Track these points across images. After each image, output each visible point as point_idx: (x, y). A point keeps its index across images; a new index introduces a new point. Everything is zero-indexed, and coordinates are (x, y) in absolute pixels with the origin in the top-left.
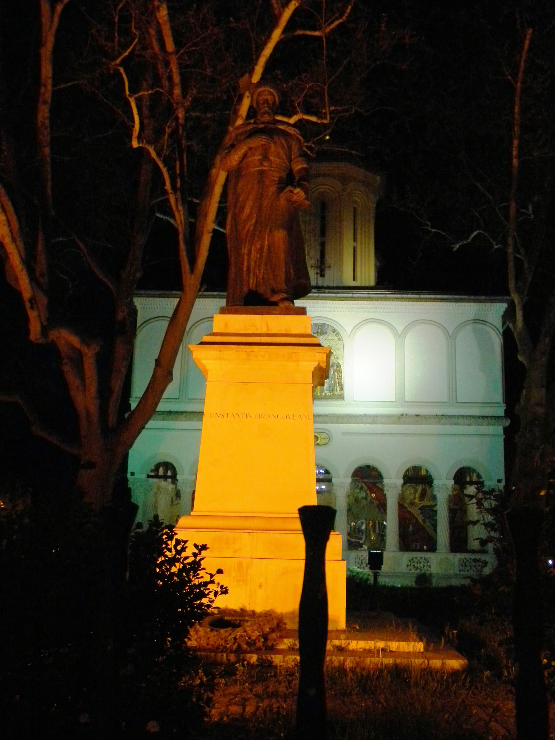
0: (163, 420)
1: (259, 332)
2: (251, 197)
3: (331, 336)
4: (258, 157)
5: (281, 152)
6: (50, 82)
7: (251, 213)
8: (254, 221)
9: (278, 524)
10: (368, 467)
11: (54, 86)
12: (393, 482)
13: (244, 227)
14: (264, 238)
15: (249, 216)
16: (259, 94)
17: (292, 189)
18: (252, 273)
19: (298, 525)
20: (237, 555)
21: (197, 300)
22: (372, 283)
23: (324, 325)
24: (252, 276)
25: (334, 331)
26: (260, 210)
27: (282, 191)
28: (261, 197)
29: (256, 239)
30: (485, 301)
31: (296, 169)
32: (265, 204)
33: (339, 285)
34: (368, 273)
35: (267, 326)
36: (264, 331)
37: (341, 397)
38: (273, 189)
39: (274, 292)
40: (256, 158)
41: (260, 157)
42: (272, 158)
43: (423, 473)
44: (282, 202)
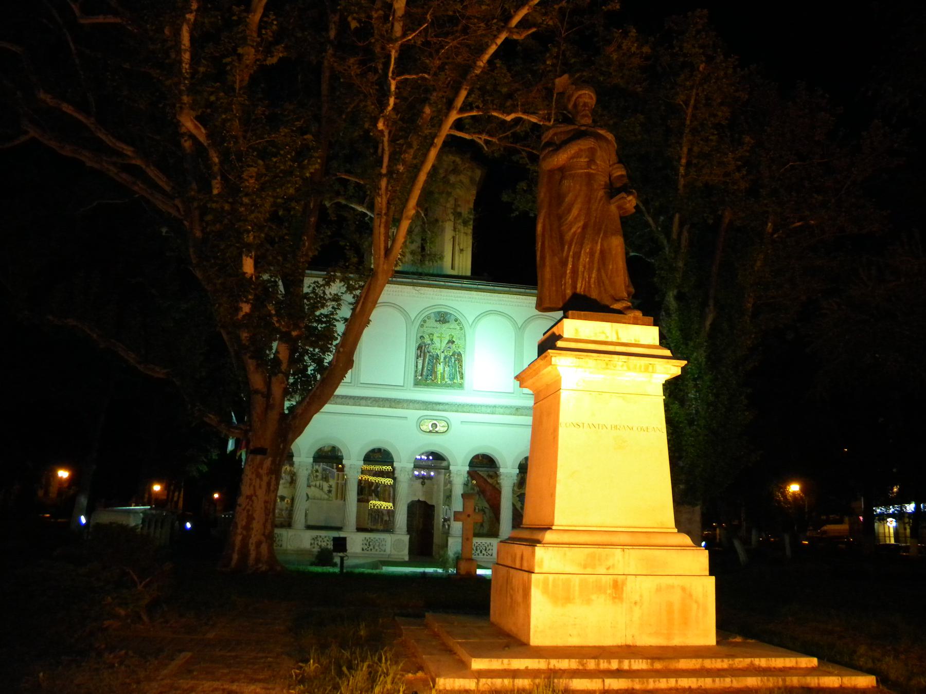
1: (609, 340)
2: (579, 200)
3: (453, 325)
4: (584, 160)
8: (581, 224)
9: (643, 540)
13: (570, 229)
14: (597, 243)
15: (576, 219)
16: (580, 97)
20: (611, 571)
22: (469, 273)
23: (446, 313)
25: (456, 320)
28: (589, 200)
29: (586, 241)
33: (439, 273)
34: (464, 264)
35: (617, 334)
36: (614, 340)
37: (461, 386)
38: (601, 193)
39: (617, 300)
41: (587, 160)
44: (613, 208)
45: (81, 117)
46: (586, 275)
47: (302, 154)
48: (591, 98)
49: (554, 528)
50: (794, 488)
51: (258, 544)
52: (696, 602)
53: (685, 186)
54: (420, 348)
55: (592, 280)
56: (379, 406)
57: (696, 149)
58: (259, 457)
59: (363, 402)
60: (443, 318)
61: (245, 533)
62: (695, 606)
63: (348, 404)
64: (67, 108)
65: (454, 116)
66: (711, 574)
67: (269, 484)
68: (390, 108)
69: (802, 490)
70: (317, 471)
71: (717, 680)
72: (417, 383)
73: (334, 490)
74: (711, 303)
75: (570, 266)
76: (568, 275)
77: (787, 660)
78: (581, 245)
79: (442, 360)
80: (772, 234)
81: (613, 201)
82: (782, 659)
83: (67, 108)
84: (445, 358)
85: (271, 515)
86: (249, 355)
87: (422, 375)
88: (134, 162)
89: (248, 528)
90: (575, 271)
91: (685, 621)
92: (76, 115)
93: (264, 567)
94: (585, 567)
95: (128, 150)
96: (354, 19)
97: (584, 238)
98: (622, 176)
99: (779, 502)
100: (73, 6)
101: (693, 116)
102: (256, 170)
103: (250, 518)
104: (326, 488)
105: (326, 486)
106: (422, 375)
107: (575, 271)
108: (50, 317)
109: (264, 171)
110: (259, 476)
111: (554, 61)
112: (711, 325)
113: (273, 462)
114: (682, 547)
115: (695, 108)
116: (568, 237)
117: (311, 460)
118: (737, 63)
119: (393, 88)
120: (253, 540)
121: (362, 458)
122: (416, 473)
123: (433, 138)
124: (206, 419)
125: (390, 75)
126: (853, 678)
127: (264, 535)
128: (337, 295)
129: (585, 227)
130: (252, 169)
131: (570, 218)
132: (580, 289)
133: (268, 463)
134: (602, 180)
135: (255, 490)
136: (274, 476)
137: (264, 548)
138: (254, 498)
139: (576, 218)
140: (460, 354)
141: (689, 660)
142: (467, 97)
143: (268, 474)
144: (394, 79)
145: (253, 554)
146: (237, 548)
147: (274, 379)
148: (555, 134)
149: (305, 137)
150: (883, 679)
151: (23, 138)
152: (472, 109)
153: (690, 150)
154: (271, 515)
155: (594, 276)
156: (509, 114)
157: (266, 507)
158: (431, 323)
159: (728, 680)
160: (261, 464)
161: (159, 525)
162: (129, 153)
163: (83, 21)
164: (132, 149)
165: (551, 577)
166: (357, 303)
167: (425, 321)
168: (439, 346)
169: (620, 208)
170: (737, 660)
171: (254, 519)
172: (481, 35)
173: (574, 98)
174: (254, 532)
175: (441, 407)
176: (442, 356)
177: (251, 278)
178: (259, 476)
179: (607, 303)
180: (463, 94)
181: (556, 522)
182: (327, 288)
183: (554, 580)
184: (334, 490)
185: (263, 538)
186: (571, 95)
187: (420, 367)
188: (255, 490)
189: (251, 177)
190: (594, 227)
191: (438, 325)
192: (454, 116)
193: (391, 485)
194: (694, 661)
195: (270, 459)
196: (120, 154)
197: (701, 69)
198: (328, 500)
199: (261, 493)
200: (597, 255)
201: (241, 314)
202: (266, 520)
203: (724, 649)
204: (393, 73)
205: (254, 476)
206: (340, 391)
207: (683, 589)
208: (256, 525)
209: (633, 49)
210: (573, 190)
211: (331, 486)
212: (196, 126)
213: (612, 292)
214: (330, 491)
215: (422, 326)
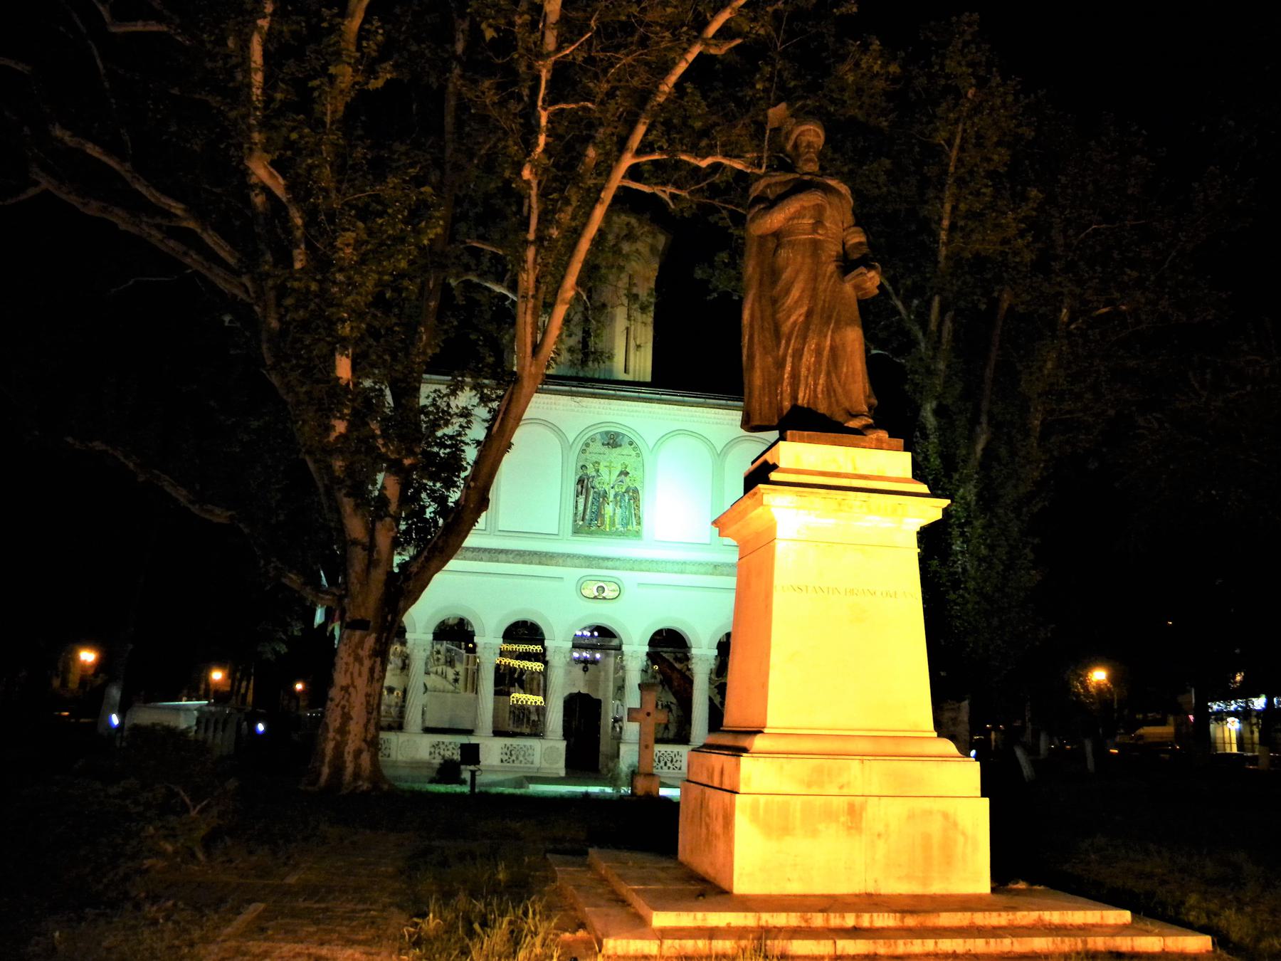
2: (802, 277)
3: (626, 450)
4: (808, 221)
7: (800, 298)
8: (804, 310)
12: (636, 650)
13: (789, 317)
14: (826, 336)
15: (797, 303)
16: (802, 133)
20: (845, 791)
22: (648, 379)
23: (618, 434)
26: (813, 297)
28: (814, 278)
29: (811, 334)
31: (851, 242)
32: (822, 287)
34: (642, 365)
36: (850, 470)
38: (831, 267)
39: (854, 416)
41: (811, 221)
44: (848, 288)
46: (811, 380)
47: (417, 213)
49: (766, 731)
51: (358, 753)
52: (964, 834)
53: (947, 257)
54: (581, 481)
56: (524, 563)
58: (358, 633)
59: (503, 556)
60: (612, 440)
61: (338, 737)
63: (481, 560)
64: (93, 150)
65: (628, 160)
66: (983, 795)
67: (372, 670)
68: (539, 150)
70: (438, 652)
71: (992, 941)
72: (577, 531)
73: (462, 678)
74: (984, 419)
75: (788, 368)
76: (786, 382)
77: (1089, 913)
79: (611, 498)
80: (1069, 324)
83: (93, 150)
84: (616, 496)
86: (344, 491)
87: (583, 519)
88: (185, 224)
89: (343, 731)
90: (795, 376)
92: (105, 159)
93: (365, 786)
94: (809, 785)
95: (178, 208)
96: (490, 26)
98: (861, 244)
99: (1078, 695)
100: (101, 8)
101: (959, 160)
102: (354, 235)
103: (346, 718)
104: (451, 676)
105: (450, 673)
106: (583, 519)
107: (795, 376)
108: (70, 440)
109: (365, 237)
111: (767, 84)
112: (983, 450)
113: (378, 640)
114: (943, 757)
115: (962, 149)
116: (785, 329)
117: (431, 637)
119: (543, 122)
120: (350, 748)
123: (600, 191)
126: (1180, 938)
127: (365, 740)
129: (809, 314)
130: (348, 234)
131: (790, 301)
132: (802, 400)
133: (370, 641)
134: (833, 249)
136: (379, 660)
137: (365, 758)
138: (351, 690)
139: (796, 302)
140: (636, 491)
142: (646, 134)
143: (370, 657)
144: (545, 109)
145: (350, 768)
146: (327, 759)
147: (378, 525)
148: (768, 186)
149: (423, 189)
151: (32, 192)
152: (652, 151)
153: (954, 208)
155: (821, 381)
156: (704, 157)
157: (368, 702)
158: (597, 447)
159: (1007, 941)
160: (361, 643)
161: (220, 727)
162: (179, 212)
163: (113, 29)
164: (182, 206)
165: (762, 799)
167: (587, 445)
168: (607, 479)
169: (857, 287)
170: (1019, 914)
172: (666, 49)
173: (793, 137)
174: (351, 737)
175: (610, 564)
176: (612, 493)
177: (348, 384)
178: (358, 659)
180: (641, 130)
181: (769, 723)
182: (452, 398)
183: (767, 804)
184: (462, 678)
185: (364, 745)
186: (791, 132)
187: (581, 508)
189: (348, 245)
190: (822, 315)
191: (606, 450)
192: (628, 160)
193: (540, 673)
195: (374, 635)
196: (168, 214)
197: (970, 95)
199: (361, 683)
200: (826, 353)
202: (368, 721)
204: (544, 101)
205: (351, 659)
206: (471, 541)
207: (945, 816)
208: (355, 728)
209: (876, 68)
210: (793, 263)
212: (271, 174)
213: (847, 405)
214: (456, 680)
215: (584, 451)
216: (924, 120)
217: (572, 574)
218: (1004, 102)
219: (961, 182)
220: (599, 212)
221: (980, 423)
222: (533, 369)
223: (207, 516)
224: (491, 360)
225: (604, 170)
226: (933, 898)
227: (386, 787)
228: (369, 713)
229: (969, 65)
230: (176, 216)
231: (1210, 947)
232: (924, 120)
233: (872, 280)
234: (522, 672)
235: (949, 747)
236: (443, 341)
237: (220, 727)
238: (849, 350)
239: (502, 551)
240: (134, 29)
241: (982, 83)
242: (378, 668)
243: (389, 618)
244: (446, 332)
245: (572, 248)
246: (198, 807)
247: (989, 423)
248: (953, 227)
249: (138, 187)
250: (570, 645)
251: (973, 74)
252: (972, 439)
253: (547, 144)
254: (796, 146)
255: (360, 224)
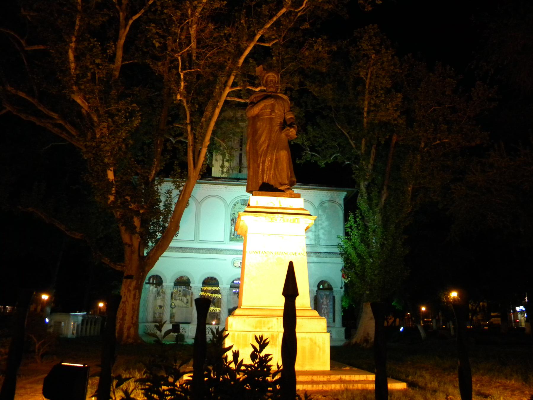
0: (176, 252)
1: (275, 206)
2: (265, 132)
4: (269, 110)
5: (281, 108)
6: (120, 60)
7: (265, 140)
10: (212, 278)
11: (122, 61)
13: (261, 148)
15: (264, 142)
16: (268, 77)
17: (289, 128)
18: (265, 173)
19: (298, 313)
20: (270, 330)
21: (196, 184)
24: (265, 175)
26: (270, 140)
27: (283, 130)
28: (270, 132)
29: (268, 154)
30: (336, 190)
36: (279, 206)
38: (277, 128)
39: (282, 185)
40: (268, 110)
42: (276, 111)
43: (185, 278)
44: (283, 135)
45: (30, 100)
46: (268, 172)
47: (132, 114)
48: (274, 77)
49: (242, 307)
50: (454, 294)
51: (129, 328)
52: (319, 347)
53: (367, 123)
54: (232, 220)
55: (271, 175)
56: (210, 253)
57: (372, 102)
58: (129, 280)
59: (201, 251)
61: (121, 322)
62: (318, 349)
63: (193, 253)
64: (22, 94)
65: (228, 90)
66: (327, 332)
67: (135, 295)
68: (182, 88)
69: (458, 295)
70: (180, 291)
71: (314, 386)
72: (231, 240)
73: (189, 301)
74: (385, 188)
75: (261, 168)
76: (260, 173)
77: (361, 376)
78: (265, 156)
80: (424, 149)
81: (283, 131)
82: (358, 376)
83: (22, 94)
85: (136, 312)
86: (121, 224)
87: (234, 235)
88: (58, 122)
89: (123, 319)
90: (263, 170)
91: (312, 357)
92: (27, 98)
93: (130, 341)
94: (256, 328)
95: (55, 116)
96: (157, 42)
97: (267, 152)
98: (291, 118)
99: (444, 302)
100: (22, 41)
101: (370, 83)
102: (106, 124)
103: (124, 314)
104: (185, 301)
105: (185, 300)
106: (234, 235)
107: (263, 170)
108: (20, 207)
109: (112, 124)
110: (129, 291)
111: (278, 58)
112: (385, 200)
113: (137, 283)
114: (312, 317)
115: (371, 79)
116: (260, 152)
117: (173, 284)
118: (393, 53)
119: (182, 77)
120: (126, 326)
121: (201, 283)
122: (234, 291)
123: (218, 102)
124: (103, 261)
125: (180, 70)
126: (393, 384)
127: (132, 323)
128: (169, 190)
129: (268, 146)
130: (104, 123)
131: (261, 142)
132: (265, 180)
133: (134, 283)
134: (278, 121)
135: (127, 298)
136: (137, 291)
137: (132, 330)
138: (126, 303)
139: (263, 142)
141: (304, 376)
142: (235, 79)
143: (134, 290)
144: (182, 72)
145: (126, 334)
146: (117, 331)
147: (133, 236)
148: (255, 98)
149: (133, 105)
150: (411, 385)
151: (4, 111)
152: (237, 86)
153: (369, 103)
154: (136, 312)
155: (272, 172)
156: (257, 87)
157: (133, 308)
159: (321, 386)
160: (130, 285)
161: (93, 324)
162: (56, 117)
163: (26, 49)
164: (57, 115)
165: (236, 333)
166: (180, 195)
167: (235, 205)
169: (287, 135)
170: (332, 376)
171: (126, 314)
172: (226, 47)
173: (265, 78)
174: (126, 322)
177: (112, 182)
178: (129, 291)
179: (278, 187)
180: (232, 78)
181: (243, 305)
182: (159, 186)
183: (238, 334)
184: (189, 301)
185: (131, 325)
186: (264, 77)
188: (127, 298)
189: (104, 127)
190: (273, 146)
192: (228, 90)
194: (307, 377)
195: (135, 281)
196: (52, 118)
197: (373, 57)
198: (186, 307)
199: (130, 300)
200: (274, 161)
201: (109, 202)
202: (133, 315)
203: (332, 372)
204: (181, 69)
205: (126, 291)
206: (172, 244)
207: (311, 340)
208: (128, 318)
209: (320, 49)
210: (262, 127)
211: (188, 300)
212: (83, 102)
213: (280, 181)
214: (187, 302)
215: (234, 208)
216: (356, 68)
217: (230, 257)
218: (388, 60)
219: (371, 93)
220: (217, 111)
221: (383, 190)
222: (194, 174)
223: (73, 236)
224: (179, 171)
225: (221, 94)
226: (304, 371)
227: (139, 341)
228: (134, 312)
229: (371, 45)
230: (54, 118)
231: (406, 387)
232: (356, 68)
233: (293, 132)
234: (214, 298)
235: (316, 313)
236: (165, 164)
237: (93, 324)
238: (282, 159)
239: (201, 249)
240: (33, 48)
241: (378, 52)
242: (137, 294)
243: (141, 274)
244: (166, 161)
245: (208, 125)
246: (40, 343)
247: (387, 189)
248: (368, 112)
249: (40, 108)
250: (229, 286)
251: (374, 49)
252: (380, 197)
253: (185, 86)
254: (266, 82)
255: (110, 120)
